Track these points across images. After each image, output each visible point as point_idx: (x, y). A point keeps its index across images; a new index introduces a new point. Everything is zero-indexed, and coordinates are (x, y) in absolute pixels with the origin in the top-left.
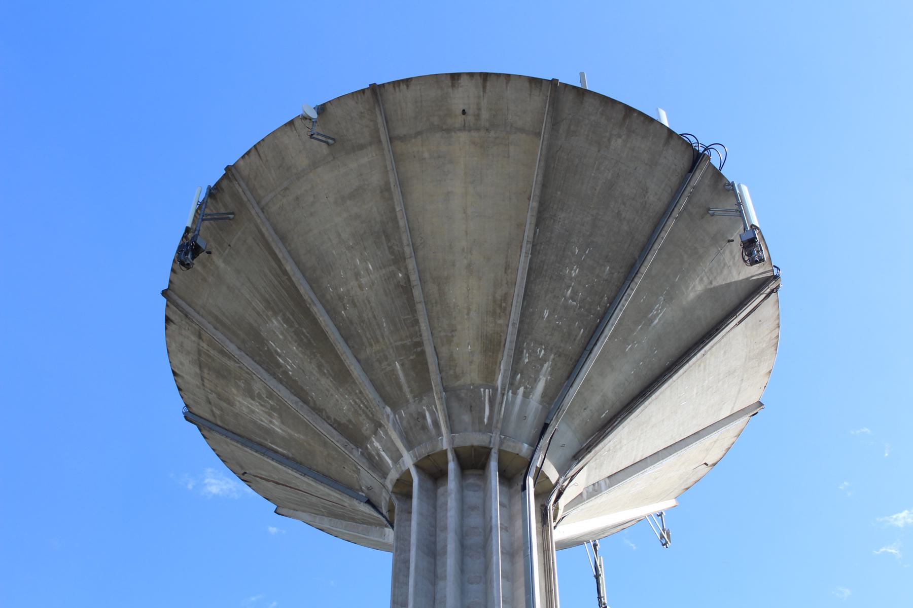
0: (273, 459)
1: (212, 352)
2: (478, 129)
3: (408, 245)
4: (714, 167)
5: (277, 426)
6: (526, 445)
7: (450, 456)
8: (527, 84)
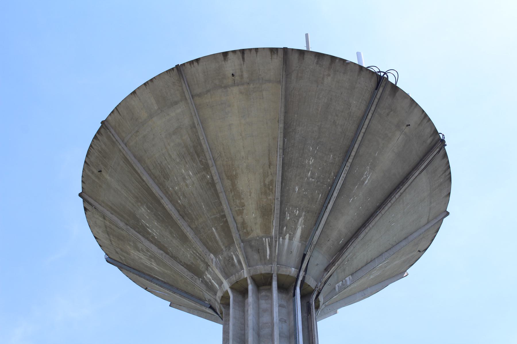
0: (157, 284)
1: (113, 227)
2: (243, 84)
3: (210, 159)
4: (392, 84)
5: (154, 266)
6: (293, 269)
7: (249, 281)
8: (269, 53)
